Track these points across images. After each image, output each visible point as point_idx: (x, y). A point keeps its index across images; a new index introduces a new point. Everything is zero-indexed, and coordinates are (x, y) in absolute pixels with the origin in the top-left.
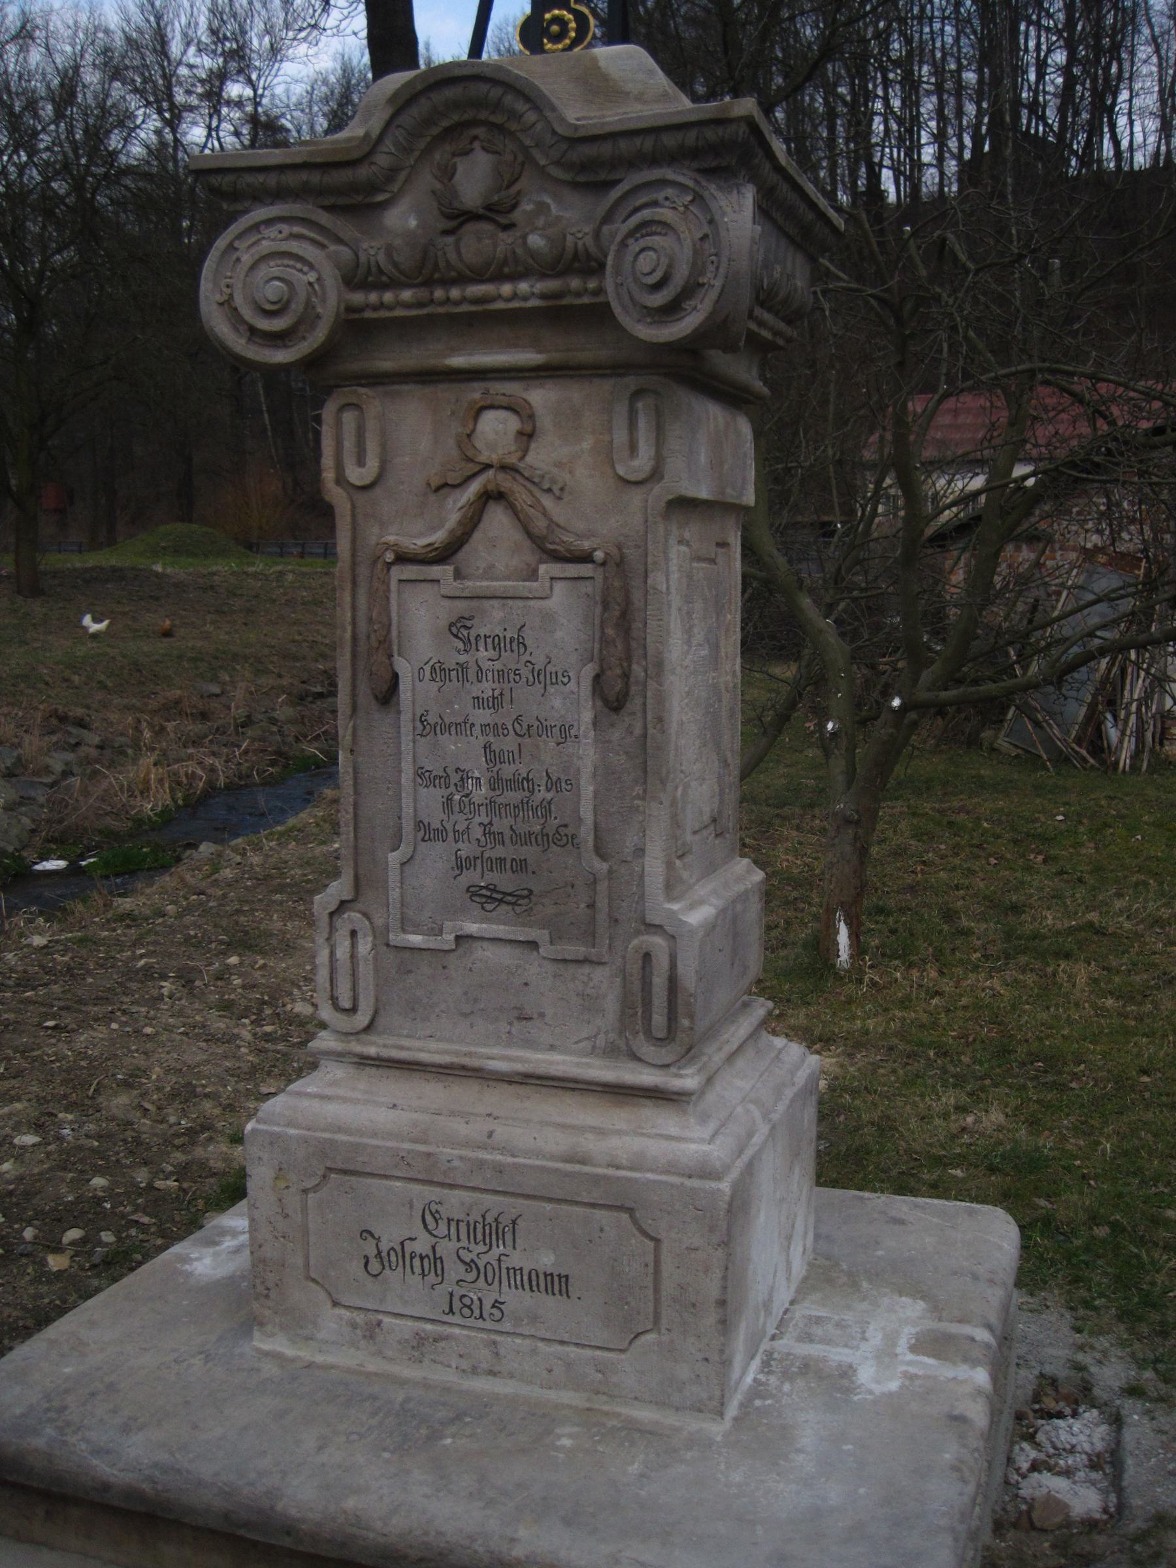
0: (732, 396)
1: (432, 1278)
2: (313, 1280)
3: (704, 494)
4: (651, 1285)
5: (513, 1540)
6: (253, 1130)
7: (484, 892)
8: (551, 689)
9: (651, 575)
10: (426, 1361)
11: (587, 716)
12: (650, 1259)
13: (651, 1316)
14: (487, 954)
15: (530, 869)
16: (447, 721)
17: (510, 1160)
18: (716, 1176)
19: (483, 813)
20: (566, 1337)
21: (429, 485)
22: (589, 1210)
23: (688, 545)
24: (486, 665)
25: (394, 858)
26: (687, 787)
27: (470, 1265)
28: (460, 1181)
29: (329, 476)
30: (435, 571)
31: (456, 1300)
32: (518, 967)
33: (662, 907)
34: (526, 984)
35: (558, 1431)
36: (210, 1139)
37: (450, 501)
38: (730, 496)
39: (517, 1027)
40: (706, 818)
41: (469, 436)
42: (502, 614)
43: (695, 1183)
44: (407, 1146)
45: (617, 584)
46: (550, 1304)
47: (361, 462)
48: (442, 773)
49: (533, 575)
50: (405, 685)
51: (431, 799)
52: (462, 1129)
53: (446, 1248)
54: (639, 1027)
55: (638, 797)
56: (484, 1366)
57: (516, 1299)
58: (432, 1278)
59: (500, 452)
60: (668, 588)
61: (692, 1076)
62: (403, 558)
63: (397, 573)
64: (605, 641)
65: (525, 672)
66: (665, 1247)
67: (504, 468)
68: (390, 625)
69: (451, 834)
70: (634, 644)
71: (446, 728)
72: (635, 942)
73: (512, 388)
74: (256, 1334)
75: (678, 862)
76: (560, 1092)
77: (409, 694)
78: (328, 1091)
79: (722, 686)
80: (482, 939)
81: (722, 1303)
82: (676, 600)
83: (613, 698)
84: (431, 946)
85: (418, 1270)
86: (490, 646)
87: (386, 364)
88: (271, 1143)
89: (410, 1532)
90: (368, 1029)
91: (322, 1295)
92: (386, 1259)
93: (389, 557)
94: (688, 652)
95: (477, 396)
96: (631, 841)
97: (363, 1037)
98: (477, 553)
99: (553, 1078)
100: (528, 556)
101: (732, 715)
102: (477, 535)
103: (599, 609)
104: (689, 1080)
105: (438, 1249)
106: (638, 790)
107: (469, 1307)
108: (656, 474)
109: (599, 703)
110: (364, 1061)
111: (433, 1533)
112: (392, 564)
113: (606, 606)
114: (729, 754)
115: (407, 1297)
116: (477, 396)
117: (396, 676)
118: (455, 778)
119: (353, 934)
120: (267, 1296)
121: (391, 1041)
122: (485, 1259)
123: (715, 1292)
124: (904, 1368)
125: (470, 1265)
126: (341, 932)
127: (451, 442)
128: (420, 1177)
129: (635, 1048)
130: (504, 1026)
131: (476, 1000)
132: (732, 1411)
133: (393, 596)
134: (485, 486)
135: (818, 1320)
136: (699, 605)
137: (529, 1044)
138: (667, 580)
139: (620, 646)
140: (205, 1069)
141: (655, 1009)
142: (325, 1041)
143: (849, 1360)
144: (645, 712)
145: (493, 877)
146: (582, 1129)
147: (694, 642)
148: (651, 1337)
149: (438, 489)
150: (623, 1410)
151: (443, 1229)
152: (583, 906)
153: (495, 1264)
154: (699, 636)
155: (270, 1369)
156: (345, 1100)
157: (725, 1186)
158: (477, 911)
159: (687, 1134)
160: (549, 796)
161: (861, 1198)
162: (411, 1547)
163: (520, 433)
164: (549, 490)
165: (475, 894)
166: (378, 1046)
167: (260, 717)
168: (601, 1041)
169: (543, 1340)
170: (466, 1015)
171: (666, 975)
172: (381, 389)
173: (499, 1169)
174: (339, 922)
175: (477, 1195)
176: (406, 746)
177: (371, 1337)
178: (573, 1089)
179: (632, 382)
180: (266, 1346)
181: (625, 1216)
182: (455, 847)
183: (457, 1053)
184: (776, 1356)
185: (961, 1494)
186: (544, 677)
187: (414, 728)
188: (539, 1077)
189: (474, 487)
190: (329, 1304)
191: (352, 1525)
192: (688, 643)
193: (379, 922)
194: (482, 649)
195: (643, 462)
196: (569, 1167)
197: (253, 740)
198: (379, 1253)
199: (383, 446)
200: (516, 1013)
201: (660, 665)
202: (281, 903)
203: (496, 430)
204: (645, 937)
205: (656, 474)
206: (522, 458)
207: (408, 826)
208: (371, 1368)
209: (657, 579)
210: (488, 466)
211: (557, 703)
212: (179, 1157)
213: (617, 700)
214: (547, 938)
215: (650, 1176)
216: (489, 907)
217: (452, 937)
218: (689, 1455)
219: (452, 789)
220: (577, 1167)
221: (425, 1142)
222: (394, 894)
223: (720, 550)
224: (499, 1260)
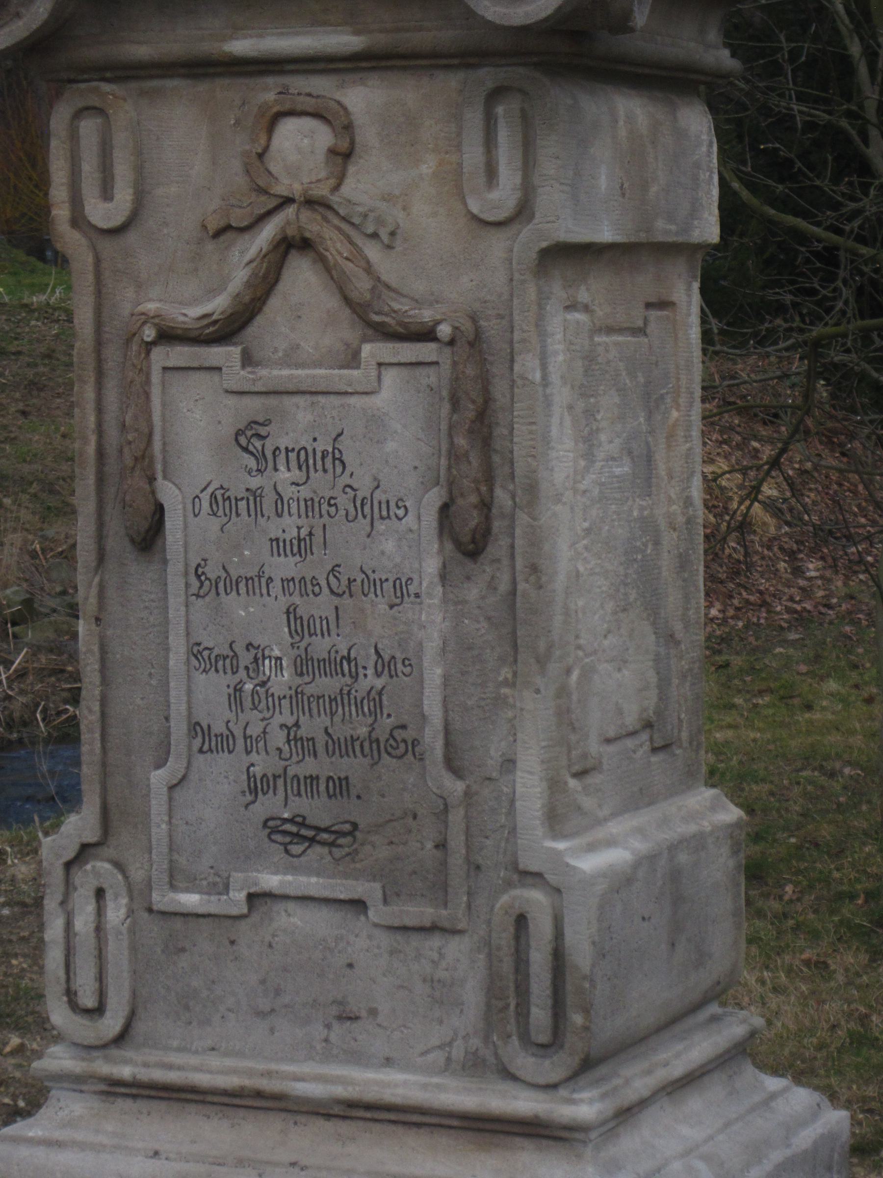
0: (666, 80)
3: (606, 235)
7: (288, 827)
8: (380, 526)
9: (518, 359)
11: (432, 566)
14: (293, 920)
15: (354, 792)
16: (234, 575)
19: (286, 710)
21: (204, 227)
23: (586, 308)
24: (288, 492)
25: (159, 778)
26: (587, 673)
29: (61, 213)
30: (216, 354)
32: (339, 939)
33: (540, 846)
34: (350, 966)
37: (235, 252)
38: (664, 230)
39: (338, 1030)
40: (631, 720)
41: (261, 156)
42: (310, 417)
45: (470, 371)
47: (107, 194)
48: (227, 652)
49: (353, 360)
50: (173, 523)
51: (212, 688)
54: (512, 1027)
55: (506, 683)
59: (306, 180)
60: (544, 377)
61: (591, 1101)
62: (168, 336)
63: (161, 357)
64: (455, 456)
65: (343, 501)
67: (310, 203)
68: (150, 435)
69: (240, 742)
70: (496, 459)
71: (233, 585)
72: (505, 899)
73: (321, 85)
75: (572, 783)
76: (400, 1130)
77: (180, 535)
78: (58, 1135)
79: (663, 524)
80: (286, 897)
82: (561, 395)
83: (470, 534)
84: (213, 910)
86: (293, 464)
87: (142, 51)
90: (121, 1039)
93: (149, 333)
94: (587, 469)
95: (271, 96)
96: (495, 752)
97: (114, 1052)
98: (275, 327)
100: (346, 331)
101: (683, 563)
102: (274, 302)
103: (446, 407)
104: (584, 1107)
106: (506, 672)
108: (523, 211)
109: (449, 546)
110: (115, 1089)
112: (154, 343)
113: (455, 403)
114: (678, 627)
116: (271, 96)
117: (160, 509)
118: (246, 658)
119: (100, 893)
121: (154, 1056)
126: (81, 891)
127: (237, 165)
129: (505, 1060)
130: (318, 1031)
131: (278, 992)
133: (156, 392)
134: (283, 229)
136: (609, 401)
137: (356, 1057)
138: (544, 367)
139: (475, 461)
141: (534, 999)
142: (58, 1059)
144: (512, 557)
145: (302, 805)
147: (600, 455)
149: (217, 234)
152: (429, 845)
154: (609, 443)
156: (82, 1146)
158: (277, 853)
160: (379, 683)
163: (332, 152)
164: (375, 236)
165: (275, 831)
166: (136, 1064)
167: (52, 603)
168: (458, 1052)
170: (261, 1014)
171: (549, 948)
172: (134, 85)
174: (78, 877)
176: (176, 603)
178: (418, 1125)
179: (488, 76)
182: (246, 760)
183: (250, 1073)
186: (371, 509)
187: (187, 585)
188: (369, 1107)
189: (268, 232)
192: (589, 456)
193: (137, 875)
194: (282, 468)
195: (504, 196)
197: (36, 650)
199: (139, 170)
200: (334, 1010)
201: (532, 489)
203: (299, 145)
204: (517, 892)
205: (523, 211)
206: (336, 188)
207: (179, 729)
209: (528, 365)
210: (288, 201)
211: (389, 546)
213: (473, 541)
214: (379, 894)
216: (296, 849)
217: (242, 896)
219: (242, 673)
222: (159, 830)
223: (654, 314)
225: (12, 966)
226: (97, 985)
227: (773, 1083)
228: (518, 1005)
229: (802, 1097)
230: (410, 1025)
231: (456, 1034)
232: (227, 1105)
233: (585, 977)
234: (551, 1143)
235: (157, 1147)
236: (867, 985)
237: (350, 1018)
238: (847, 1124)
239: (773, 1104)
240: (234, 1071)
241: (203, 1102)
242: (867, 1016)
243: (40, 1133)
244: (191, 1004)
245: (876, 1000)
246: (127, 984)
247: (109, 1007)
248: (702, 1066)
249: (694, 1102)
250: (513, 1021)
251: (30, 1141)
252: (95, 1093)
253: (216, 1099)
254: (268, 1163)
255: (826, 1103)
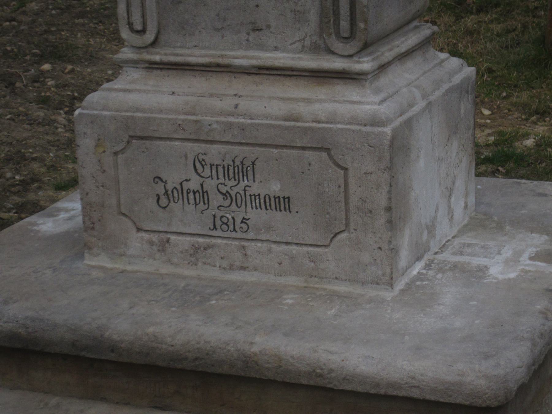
1: (201, 206)
2: (124, 214)
4: (343, 200)
5: (252, 343)
6: (80, 114)
10: (200, 264)
12: (341, 181)
13: (344, 221)
17: (249, 121)
18: (382, 124)
20: (290, 240)
22: (301, 152)
27: (226, 195)
28: (218, 138)
31: (218, 219)
35: (285, 297)
36: (39, 188)
43: (369, 129)
44: (182, 117)
46: (279, 216)
52: (217, 104)
53: (210, 185)
54: (332, 30)
56: (238, 263)
57: (257, 216)
58: (201, 206)
61: (368, 62)
66: (351, 173)
74: (87, 255)
76: (282, 78)
78: (128, 87)
81: (389, 209)
85: (192, 201)
88: (92, 122)
89: (188, 342)
90: (154, 43)
91: (130, 224)
92: (171, 196)
97: (151, 50)
99: (277, 69)
104: (365, 64)
105: (204, 186)
107: (226, 224)
111: (202, 342)
115: (187, 219)
120: (93, 229)
122: (236, 190)
123: (384, 202)
124: (522, 267)
125: (226, 195)
128: (191, 137)
129: (329, 45)
130: (244, 36)
131: (225, 20)
132: (400, 285)
135: (469, 245)
137: (261, 47)
140: (31, 142)
142: (126, 54)
143: (485, 264)
146: (296, 100)
148: (344, 235)
150: (329, 287)
151: (207, 172)
153: (242, 193)
155: (95, 274)
156: (139, 91)
157: (388, 130)
159: (364, 99)
161: (519, 183)
162: (189, 351)
168: (307, 43)
169: (276, 242)
170: (218, 30)
173: (243, 128)
175: (230, 147)
177: (163, 250)
180: (94, 263)
181: (324, 155)
183: (213, 56)
184: (435, 261)
185: (544, 325)
188: (268, 69)
190: (135, 230)
191: (152, 342)
196: (288, 124)
198: (166, 192)
200: (251, 27)
202: (83, 25)
208: (163, 271)
212: (17, 199)
215: (339, 126)
218: (368, 306)
220: (293, 124)
221: (194, 114)
224: (245, 190)
225: (62, 35)
226: (142, 20)
227: (443, 56)
228: (334, 20)
229: (455, 62)
230: (285, 31)
231: (306, 34)
232: (203, 71)
233: (364, 6)
234: (350, 81)
235: (173, 90)
236: (455, 31)
237: (258, 30)
238: (474, 73)
239: (443, 64)
240: (206, 56)
241: (193, 70)
242: (456, 44)
243: (120, 86)
244: (185, 26)
245: (459, 37)
246: (155, 18)
247: (148, 29)
248: (413, 47)
249: (409, 64)
250: (332, 27)
251: (116, 90)
252: (143, 68)
253: (198, 68)
254: (224, 95)
255: (465, 64)
